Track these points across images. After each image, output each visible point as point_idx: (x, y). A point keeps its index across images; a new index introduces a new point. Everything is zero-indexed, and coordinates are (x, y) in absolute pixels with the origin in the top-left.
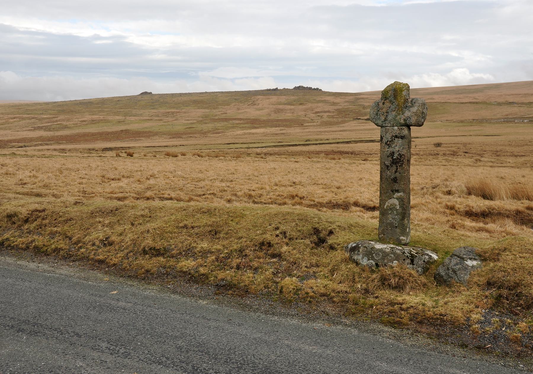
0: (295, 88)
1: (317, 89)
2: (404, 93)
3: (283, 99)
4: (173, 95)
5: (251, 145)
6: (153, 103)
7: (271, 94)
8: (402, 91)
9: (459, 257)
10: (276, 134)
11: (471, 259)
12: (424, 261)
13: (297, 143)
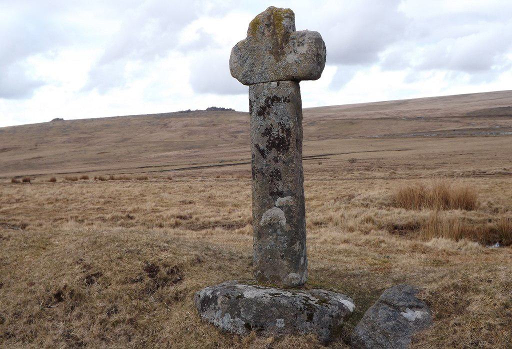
0: (208, 109)
1: (230, 109)
2: (285, 22)
3: (196, 120)
4: (84, 121)
5: (164, 169)
6: (65, 129)
7: (184, 116)
8: (281, 19)
9: (390, 305)
10: (191, 156)
11: (411, 307)
12: (332, 316)
13: (212, 164)
